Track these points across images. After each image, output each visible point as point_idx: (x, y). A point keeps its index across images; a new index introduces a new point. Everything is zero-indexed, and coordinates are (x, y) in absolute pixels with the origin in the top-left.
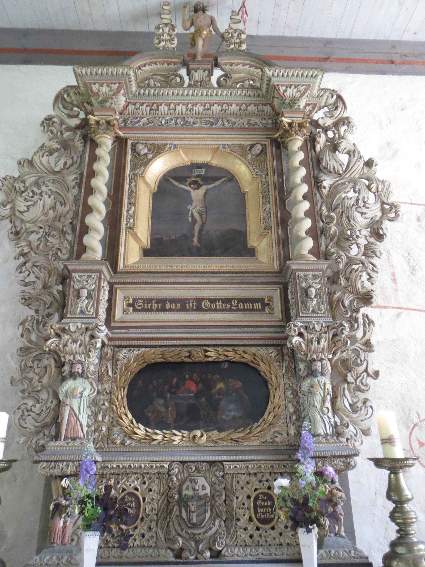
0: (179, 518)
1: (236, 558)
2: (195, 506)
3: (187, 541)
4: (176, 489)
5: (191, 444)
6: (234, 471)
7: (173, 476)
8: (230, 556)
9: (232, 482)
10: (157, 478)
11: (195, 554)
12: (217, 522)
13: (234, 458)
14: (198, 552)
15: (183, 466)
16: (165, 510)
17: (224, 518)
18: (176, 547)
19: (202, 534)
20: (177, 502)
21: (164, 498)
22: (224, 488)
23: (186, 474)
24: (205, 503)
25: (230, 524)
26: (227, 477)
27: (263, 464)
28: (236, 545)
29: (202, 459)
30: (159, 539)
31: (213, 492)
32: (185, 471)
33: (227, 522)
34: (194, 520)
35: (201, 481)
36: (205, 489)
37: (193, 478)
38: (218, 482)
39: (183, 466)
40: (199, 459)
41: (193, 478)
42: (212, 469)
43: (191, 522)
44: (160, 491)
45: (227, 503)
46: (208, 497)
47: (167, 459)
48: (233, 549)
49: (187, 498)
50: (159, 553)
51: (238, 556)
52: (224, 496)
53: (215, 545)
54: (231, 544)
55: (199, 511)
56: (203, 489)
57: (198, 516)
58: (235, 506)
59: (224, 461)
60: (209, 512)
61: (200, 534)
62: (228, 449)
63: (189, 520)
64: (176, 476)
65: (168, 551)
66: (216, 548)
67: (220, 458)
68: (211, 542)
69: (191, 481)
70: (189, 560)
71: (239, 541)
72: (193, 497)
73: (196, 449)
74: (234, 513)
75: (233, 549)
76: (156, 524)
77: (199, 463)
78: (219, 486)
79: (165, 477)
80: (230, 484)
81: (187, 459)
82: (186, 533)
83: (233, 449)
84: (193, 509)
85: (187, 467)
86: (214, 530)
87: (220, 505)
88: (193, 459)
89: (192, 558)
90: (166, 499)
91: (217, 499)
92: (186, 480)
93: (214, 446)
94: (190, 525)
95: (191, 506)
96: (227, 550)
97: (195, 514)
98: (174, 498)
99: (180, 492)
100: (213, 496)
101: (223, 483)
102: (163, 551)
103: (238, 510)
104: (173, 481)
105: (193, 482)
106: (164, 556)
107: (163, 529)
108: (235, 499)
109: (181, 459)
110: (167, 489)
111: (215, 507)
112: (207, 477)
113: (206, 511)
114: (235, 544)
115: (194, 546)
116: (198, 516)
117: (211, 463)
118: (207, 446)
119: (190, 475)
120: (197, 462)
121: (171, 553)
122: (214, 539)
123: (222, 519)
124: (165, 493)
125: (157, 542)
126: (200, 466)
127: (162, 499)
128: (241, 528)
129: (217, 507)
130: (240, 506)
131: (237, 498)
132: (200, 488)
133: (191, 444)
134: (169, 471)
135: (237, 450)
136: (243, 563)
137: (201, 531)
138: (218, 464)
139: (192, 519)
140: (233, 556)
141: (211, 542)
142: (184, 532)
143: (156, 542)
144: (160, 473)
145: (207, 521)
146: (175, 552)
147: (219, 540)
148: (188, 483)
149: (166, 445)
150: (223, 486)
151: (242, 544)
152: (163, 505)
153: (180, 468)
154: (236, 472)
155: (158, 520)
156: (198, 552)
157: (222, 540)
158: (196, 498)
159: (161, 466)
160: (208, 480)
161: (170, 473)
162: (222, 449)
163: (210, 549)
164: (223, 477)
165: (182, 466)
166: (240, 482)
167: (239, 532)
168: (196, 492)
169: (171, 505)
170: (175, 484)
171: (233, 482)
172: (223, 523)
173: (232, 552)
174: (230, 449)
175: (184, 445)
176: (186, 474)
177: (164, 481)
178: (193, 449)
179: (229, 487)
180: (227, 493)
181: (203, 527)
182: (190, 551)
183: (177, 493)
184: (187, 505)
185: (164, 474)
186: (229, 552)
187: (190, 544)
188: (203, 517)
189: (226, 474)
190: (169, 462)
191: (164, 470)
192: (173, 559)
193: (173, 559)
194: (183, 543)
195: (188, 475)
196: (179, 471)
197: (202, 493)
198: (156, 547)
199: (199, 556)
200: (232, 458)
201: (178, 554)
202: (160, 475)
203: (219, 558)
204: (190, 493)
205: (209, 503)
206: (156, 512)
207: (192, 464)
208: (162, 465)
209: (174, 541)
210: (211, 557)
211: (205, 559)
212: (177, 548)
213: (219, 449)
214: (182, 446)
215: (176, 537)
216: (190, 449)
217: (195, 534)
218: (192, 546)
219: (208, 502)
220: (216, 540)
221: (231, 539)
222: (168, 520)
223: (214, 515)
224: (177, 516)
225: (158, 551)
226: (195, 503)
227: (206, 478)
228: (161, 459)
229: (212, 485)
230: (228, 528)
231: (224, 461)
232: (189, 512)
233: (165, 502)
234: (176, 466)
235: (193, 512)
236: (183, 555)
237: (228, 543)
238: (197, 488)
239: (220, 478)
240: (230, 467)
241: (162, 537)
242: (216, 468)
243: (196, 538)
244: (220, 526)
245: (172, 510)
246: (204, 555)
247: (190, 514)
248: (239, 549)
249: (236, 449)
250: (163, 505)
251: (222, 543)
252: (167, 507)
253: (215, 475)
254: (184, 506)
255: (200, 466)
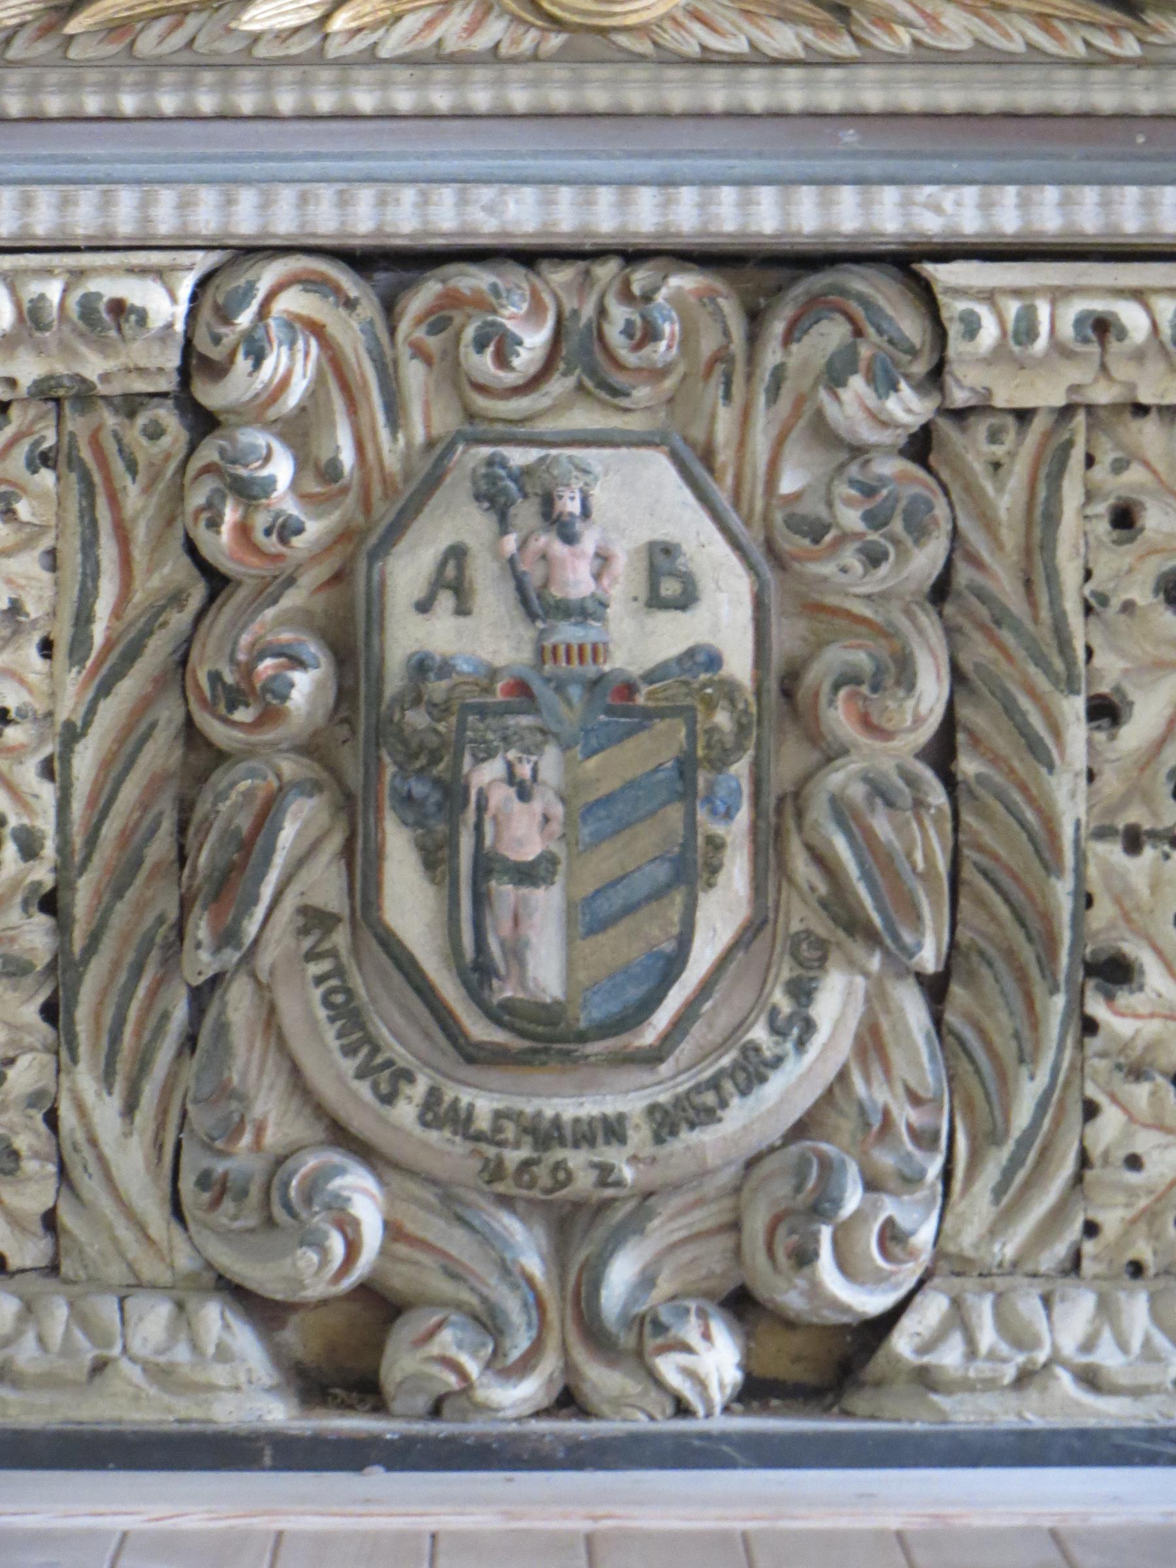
0: (340, 938)
1: (1067, 1404)
2: (545, 801)
3: (451, 1203)
4: (292, 599)
5: (494, 31)
6: (1074, 374)
7: (256, 438)
8: (990, 1384)
9: (1043, 518)
10: (46, 459)
11: (550, 1364)
12: (836, 1001)
13: (1088, 213)
14: (595, 1335)
15: (390, 307)
16: (161, 847)
17: (929, 959)
18: (313, 1272)
19: (639, 1137)
20: (310, 748)
21: (145, 704)
22: (941, 591)
23: (427, 412)
24: (686, 767)
25: (1002, 1024)
26: (973, 448)
27: (990, 296)
28: (1074, 1264)
29: (644, 216)
30: (91, 1185)
31: (787, 636)
32: (414, 375)
33: (957, 990)
34: (546, 971)
35: (635, 499)
36: (686, 601)
37: (519, 457)
38: (851, 518)
39: (390, 307)
40: (604, 217)
41: (519, 457)
42: (772, 355)
43: (507, 992)
44: (84, 618)
45: (968, 766)
46: (729, 690)
47: (165, 223)
48: (1029, 1306)
49: (440, 710)
50: (99, 1337)
51: (1090, 1379)
52: (931, 691)
53: (804, 1257)
54: (1007, 1249)
55: (605, 863)
56: (656, 602)
57: (598, 926)
58: (1071, 806)
59: (946, 253)
60: (736, 872)
61: (613, 1130)
62: (992, 99)
63: (478, 974)
64: (299, 431)
65: (214, 1317)
66: (815, 1289)
67: (887, 214)
68: (757, 1223)
69: (494, 498)
70: (476, 1427)
71: (1111, 1220)
72: (521, 688)
73: (560, 99)
74: (1063, 891)
75: (1029, 1306)
76: (50, 1012)
77: (607, 270)
78: (874, 558)
79: (145, 450)
80: (1011, 539)
81: (444, 216)
82: (436, 1112)
83: (1066, 98)
84: (524, 834)
85: (438, 320)
86: (790, 1088)
87: (879, 791)
88: (519, 215)
89: (516, 1397)
90: (168, 714)
91: (839, 718)
92: (432, 482)
93: (812, 61)
94: (480, 1030)
95: (501, 795)
96: (959, 1317)
97: (546, 905)
98: (271, 715)
99: (349, 640)
100: (787, 690)
101: (919, 530)
102: (153, 1321)
103: (1113, 852)
104: (249, 492)
105: (526, 512)
106: (162, 1374)
107: (143, 1064)
108: (1077, 731)
109: (362, 219)
110: (176, 599)
111: (819, 812)
112: (707, 456)
113: (692, 868)
114: (1060, 1250)
115: (533, 1264)
116: (588, 920)
117: (765, 273)
118: (707, 59)
119: (475, 428)
120: (580, 254)
121: (245, 1340)
122: (796, 1185)
123: (899, 961)
124: (158, 650)
125: (66, 1218)
126: (619, 313)
127: (111, 711)
128: (1137, 1073)
129: (842, 812)
130: (1135, 815)
131: (1106, 712)
132: (625, 582)
133: (494, 31)
134: (195, 364)
135: (1127, 117)
136: (1151, 1460)
137: (628, 1099)
138: (860, 282)
139: (516, 952)
140: (1025, 1378)
141: (757, 1223)
142: (406, 1112)
143: (50, 1221)
144: (85, 396)
145: (705, 989)
146: (290, 1335)
147: (853, 1199)
148: (456, 521)
149: (148, 43)
150: (927, 560)
151: (1143, 1250)
152: (130, 792)
153: (350, 333)
154: (1103, 395)
155: (64, 969)
156: (595, 1335)
157: (889, 1208)
158: (570, 710)
159: (88, 306)
160: (722, 496)
161: (211, 396)
162: (912, 99)
163: (741, 1305)
164: (920, 446)
165: (370, 308)
166: (1155, 520)
167: (1111, 1120)
168: (568, 633)
169: (231, 799)
170: (287, 530)
171: (1052, 518)
172: (914, 1010)
173: (1017, 1335)
174: (1028, 99)
175: (393, 43)
176: (427, 412)
177: (133, 496)
178: (520, 99)
179: (1005, 584)
180: (978, 652)
181: (653, 1057)
182: (489, 1323)
183: (312, 648)
184: (453, 794)
185: (131, 404)
186: (987, 1337)
187: (487, 1239)
188: (657, 930)
189: (960, 415)
190: (204, 261)
191: (138, 352)
192: (277, 1413)
193: (277, 1413)
194: (393, 1230)
195: (446, 421)
196: (334, 361)
197: (640, 643)
198: (53, 1269)
199: (602, 1379)
200: (1048, 214)
201: (345, 1364)
202: (75, 423)
203: (860, 1402)
204: (487, 639)
205: (741, 768)
206: (43, 874)
207: (515, 276)
208: (108, 288)
209: (279, 1206)
210: (754, 1391)
211: (682, 1409)
212: (316, 1290)
213: (873, 100)
214: (370, 57)
215: (311, 1162)
216: (481, 99)
217: (545, 1135)
218: (507, 1270)
219: (721, 760)
220: (821, 1206)
221: (1010, 1199)
222: (202, 961)
223: (800, 916)
224: (315, 920)
225: (80, 1318)
226: (550, 762)
227: (696, 464)
228: (84, 219)
229: (777, 549)
230: (973, 1074)
231: (946, 253)
232: (474, 878)
233: (161, 752)
234: (292, 302)
235: (528, 875)
236: (401, 1363)
237: (968, 1238)
238: (577, 579)
239: (889, 467)
240: (1026, 331)
241: (132, 1162)
242: (831, 334)
243: (562, 1175)
244: (871, 1043)
245: (249, 849)
246: (668, 1367)
247: (481, 900)
248: (1106, 1309)
249: (1106, 100)
250: (130, 792)
251: (893, 1238)
252: (185, 808)
253: (823, 433)
254: (407, 800)
255: (619, 313)
